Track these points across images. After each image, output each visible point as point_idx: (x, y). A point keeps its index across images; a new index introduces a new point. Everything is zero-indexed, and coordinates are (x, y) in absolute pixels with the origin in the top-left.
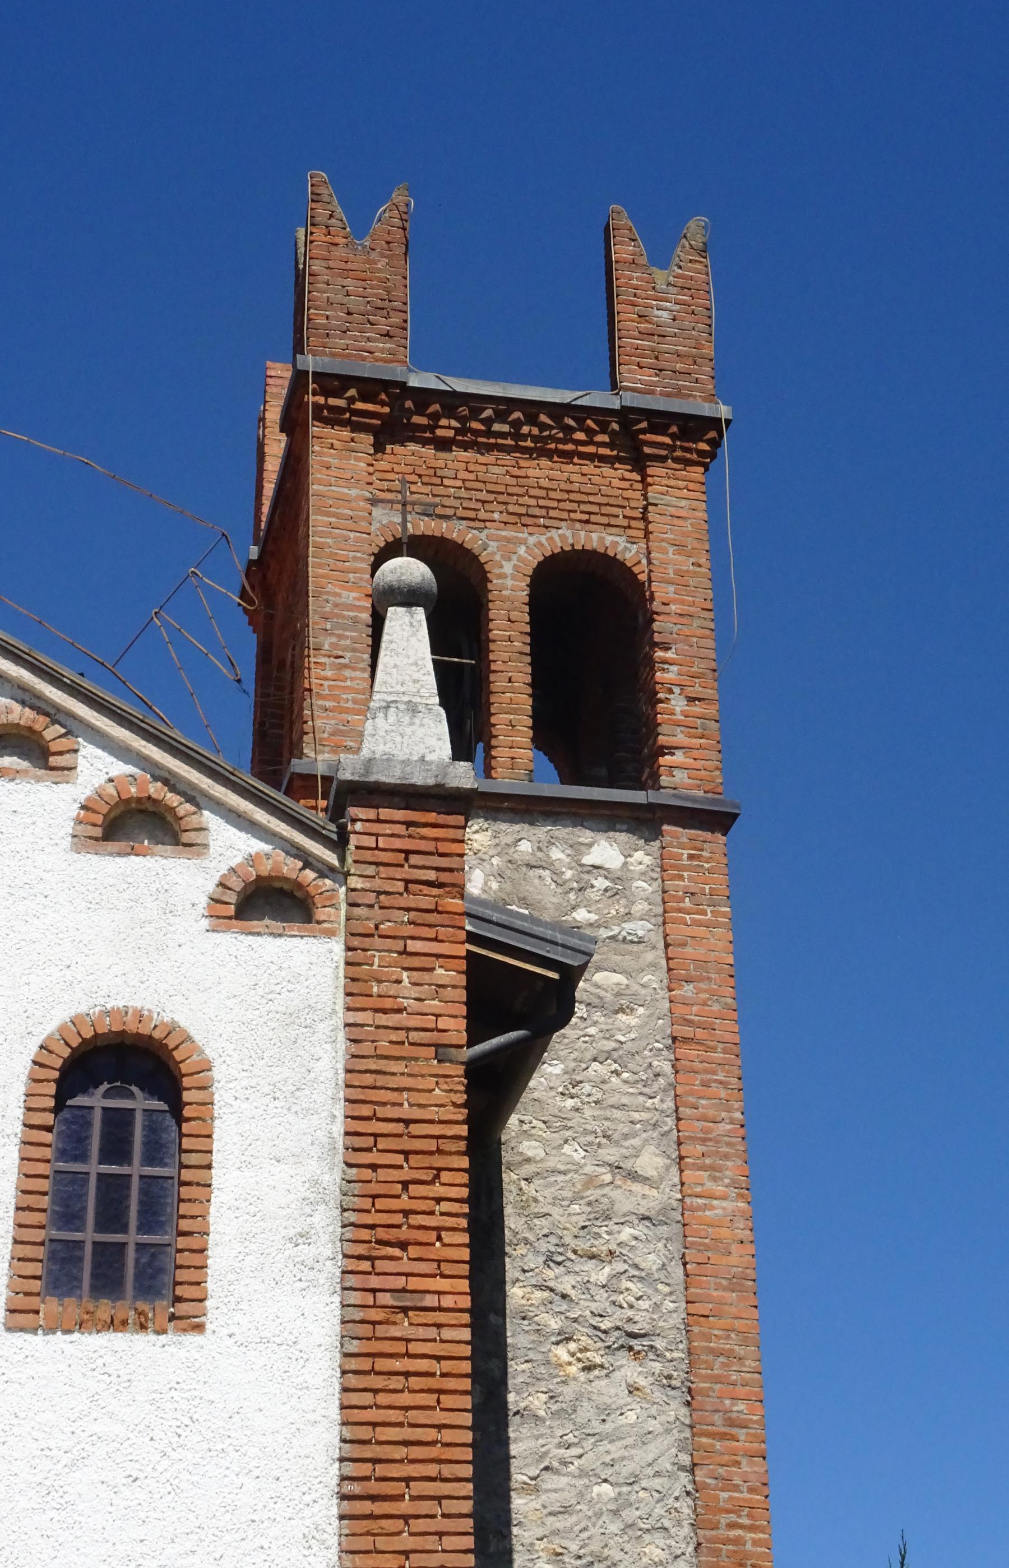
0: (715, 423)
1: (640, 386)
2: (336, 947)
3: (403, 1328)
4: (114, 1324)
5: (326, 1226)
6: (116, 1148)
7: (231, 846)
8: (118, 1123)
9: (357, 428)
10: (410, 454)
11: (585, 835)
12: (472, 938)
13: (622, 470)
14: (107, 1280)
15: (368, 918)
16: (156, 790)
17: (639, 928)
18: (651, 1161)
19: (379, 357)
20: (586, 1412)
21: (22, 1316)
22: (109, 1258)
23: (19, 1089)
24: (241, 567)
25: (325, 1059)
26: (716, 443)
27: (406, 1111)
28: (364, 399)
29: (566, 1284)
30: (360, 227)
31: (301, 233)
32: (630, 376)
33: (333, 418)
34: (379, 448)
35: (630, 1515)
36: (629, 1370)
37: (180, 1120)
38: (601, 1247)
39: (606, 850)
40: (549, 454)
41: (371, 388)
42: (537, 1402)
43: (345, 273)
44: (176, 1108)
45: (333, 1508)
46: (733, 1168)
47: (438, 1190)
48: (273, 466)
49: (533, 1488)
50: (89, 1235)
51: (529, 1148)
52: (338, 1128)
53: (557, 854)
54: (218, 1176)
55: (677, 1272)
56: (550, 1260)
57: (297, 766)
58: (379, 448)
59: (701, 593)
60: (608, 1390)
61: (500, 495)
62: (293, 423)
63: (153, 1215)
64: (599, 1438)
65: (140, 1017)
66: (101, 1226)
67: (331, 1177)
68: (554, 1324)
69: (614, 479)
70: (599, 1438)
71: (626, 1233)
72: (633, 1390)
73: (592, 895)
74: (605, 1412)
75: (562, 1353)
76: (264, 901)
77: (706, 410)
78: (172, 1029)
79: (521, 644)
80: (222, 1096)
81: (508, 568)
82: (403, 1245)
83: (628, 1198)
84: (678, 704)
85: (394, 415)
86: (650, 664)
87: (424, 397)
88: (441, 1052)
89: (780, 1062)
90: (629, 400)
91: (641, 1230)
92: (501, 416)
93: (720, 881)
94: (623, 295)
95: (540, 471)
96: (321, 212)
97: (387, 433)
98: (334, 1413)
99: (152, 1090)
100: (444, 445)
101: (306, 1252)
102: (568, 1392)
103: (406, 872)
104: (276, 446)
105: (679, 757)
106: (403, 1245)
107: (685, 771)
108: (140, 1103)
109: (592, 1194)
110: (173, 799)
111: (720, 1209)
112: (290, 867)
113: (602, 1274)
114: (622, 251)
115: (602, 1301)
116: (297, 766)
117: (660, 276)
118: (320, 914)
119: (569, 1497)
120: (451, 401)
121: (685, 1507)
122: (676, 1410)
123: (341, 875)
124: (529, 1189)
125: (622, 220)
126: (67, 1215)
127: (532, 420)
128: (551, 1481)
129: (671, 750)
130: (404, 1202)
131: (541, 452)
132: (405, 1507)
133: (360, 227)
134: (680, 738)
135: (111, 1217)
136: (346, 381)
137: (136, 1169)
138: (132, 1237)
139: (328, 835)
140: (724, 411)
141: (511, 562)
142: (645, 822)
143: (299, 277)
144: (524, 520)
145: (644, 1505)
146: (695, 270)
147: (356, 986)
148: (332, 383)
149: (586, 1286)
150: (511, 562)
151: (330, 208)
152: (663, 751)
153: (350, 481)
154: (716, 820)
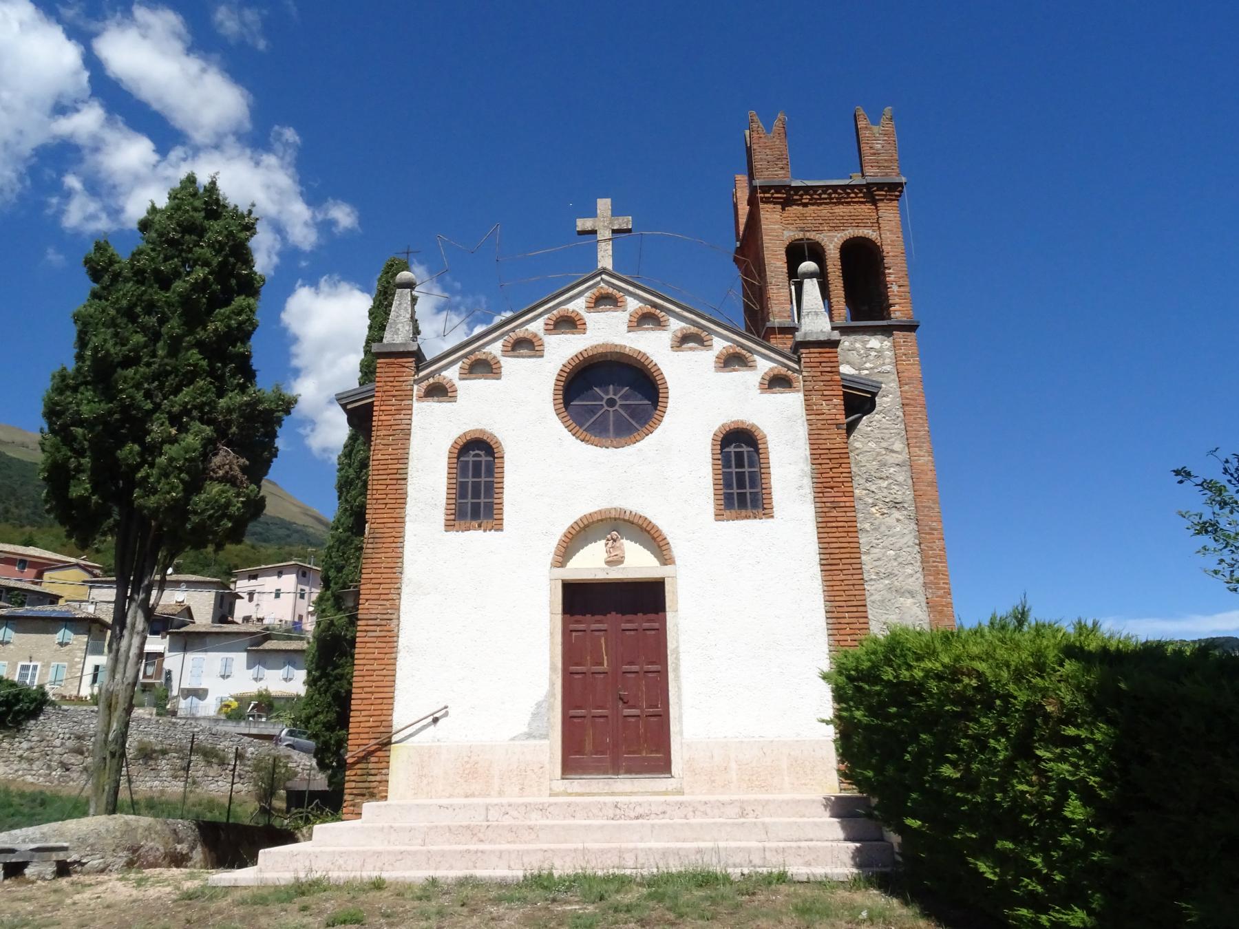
0: (901, 184)
1: (873, 174)
2: (801, 396)
3: (834, 513)
4: (747, 517)
5: (807, 483)
6: (740, 464)
7: (764, 365)
8: (739, 456)
9: (775, 203)
10: (795, 210)
11: (866, 338)
12: (844, 386)
13: (868, 206)
14: (742, 503)
15: (810, 385)
16: (738, 350)
17: (888, 368)
18: (898, 446)
19: (779, 176)
20: (883, 528)
21: (449, 526)
22: (742, 497)
23: (709, 448)
24: (733, 250)
25: (801, 431)
26: (901, 192)
27: (829, 446)
28: (777, 192)
29: (873, 488)
30: (769, 128)
31: (747, 132)
32: (869, 171)
33: (767, 201)
34: (783, 209)
35: (900, 560)
36: (896, 514)
37: (759, 454)
38: (884, 475)
39: (875, 342)
40: (842, 203)
41: (778, 189)
42: (867, 526)
43: (765, 147)
44: (757, 450)
45: (818, 568)
46: (926, 446)
47: (841, 470)
48: (743, 220)
49: (867, 553)
50: (735, 491)
51: (857, 445)
52: (808, 453)
53: (857, 345)
54: (772, 470)
55: (910, 481)
56: (867, 480)
57: (768, 324)
58: (783, 209)
59: (900, 247)
60: (890, 521)
61: (826, 220)
62: (752, 202)
63: (753, 484)
64: (888, 536)
65: (742, 422)
67: (807, 468)
68: (870, 501)
69: (866, 209)
70: (888, 536)
71: (892, 470)
72: (898, 520)
73: (871, 358)
74: (889, 528)
75: (873, 510)
76: (777, 382)
77: (897, 180)
78: (753, 425)
79: (839, 273)
80: (771, 446)
81: (831, 246)
82: (832, 488)
83: (892, 458)
84: (895, 288)
85: (788, 197)
86: (884, 275)
88: (838, 426)
89: (945, 416)
90: (870, 180)
91: (897, 469)
92: (824, 192)
93: (915, 349)
94: (863, 141)
95: (840, 210)
96: (755, 125)
97: (786, 203)
98: (816, 540)
99: (748, 445)
100: (805, 205)
101: (802, 492)
102: (877, 522)
103: (821, 369)
104: (744, 209)
105: (897, 307)
106: (832, 488)
107: (899, 313)
108: (745, 449)
109: (879, 458)
110: (744, 352)
111: (923, 460)
112: (783, 371)
113: (885, 484)
114: (861, 124)
115: (885, 492)
116: (768, 324)
117: (876, 129)
118: (795, 385)
119: (879, 555)
120: (807, 189)
121: (918, 556)
122: (913, 526)
123: (800, 372)
124: (858, 458)
125: (861, 112)
126: (728, 485)
127: (835, 192)
128: (874, 550)
129: (894, 305)
130: (831, 474)
131: (839, 203)
132: (841, 567)
133: (769, 128)
134: (897, 300)
135: (741, 484)
136: (771, 187)
137: (746, 469)
138: (748, 490)
139: (802, 360)
140: (904, 180)
141: (832, 244)
142: (887, 331)
143: (749, 151)
144: (835, 228)
145: (904, 556)
146: (889, 127)
148: (765, 189)
149: (880, 488)
150: (832, 244)
151: (758, 124)
152: (891, 305)
153: (775, 223)
154: (911, 328)
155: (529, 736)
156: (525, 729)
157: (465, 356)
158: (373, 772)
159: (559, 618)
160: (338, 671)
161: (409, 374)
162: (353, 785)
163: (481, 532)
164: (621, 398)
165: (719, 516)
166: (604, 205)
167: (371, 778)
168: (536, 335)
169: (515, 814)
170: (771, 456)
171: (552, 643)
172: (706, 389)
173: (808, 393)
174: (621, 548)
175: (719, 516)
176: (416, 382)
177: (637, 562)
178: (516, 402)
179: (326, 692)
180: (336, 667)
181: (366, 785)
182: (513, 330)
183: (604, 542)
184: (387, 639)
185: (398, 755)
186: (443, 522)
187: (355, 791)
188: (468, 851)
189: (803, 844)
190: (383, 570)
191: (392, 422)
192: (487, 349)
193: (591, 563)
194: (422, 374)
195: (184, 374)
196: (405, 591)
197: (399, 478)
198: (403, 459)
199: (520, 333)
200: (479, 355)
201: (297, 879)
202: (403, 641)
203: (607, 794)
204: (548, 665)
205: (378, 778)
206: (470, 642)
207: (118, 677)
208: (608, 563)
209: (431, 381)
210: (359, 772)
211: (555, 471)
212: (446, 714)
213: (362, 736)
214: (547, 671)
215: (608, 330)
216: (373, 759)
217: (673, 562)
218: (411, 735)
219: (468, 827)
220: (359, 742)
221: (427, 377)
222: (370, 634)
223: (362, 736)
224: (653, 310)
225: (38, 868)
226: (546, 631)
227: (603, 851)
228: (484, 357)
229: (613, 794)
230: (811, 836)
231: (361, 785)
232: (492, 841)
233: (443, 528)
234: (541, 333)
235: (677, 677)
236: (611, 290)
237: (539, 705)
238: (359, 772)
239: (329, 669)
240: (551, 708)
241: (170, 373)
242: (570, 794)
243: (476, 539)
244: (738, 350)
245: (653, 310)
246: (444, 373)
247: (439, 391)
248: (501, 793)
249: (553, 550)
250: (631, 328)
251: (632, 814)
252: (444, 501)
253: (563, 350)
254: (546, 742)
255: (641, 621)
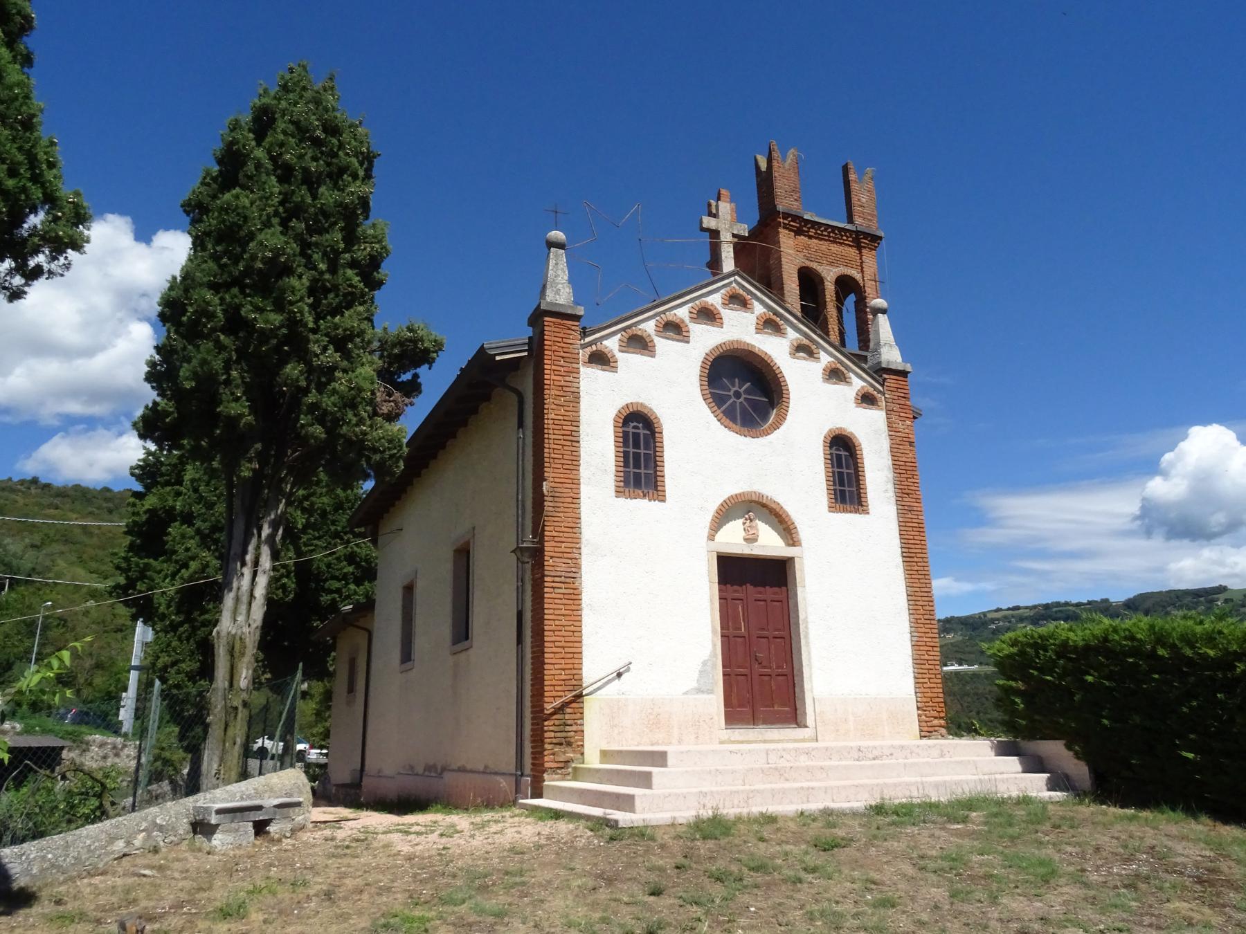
0: (881, 238)
5: (890, 487)
8: (636, 436)
15: (891, 406)
16: (839, 366)
21: (866, 512)
23: (821, 448)
32: (858, 220)
44: (653, 433)
52: (890, 462)
65: (646, 407)
66: (635, 467)
67: (891, 475)
69: (853, 252)
76: (867, 399)
80: (865, 452)
85: (802, 227)
87: (807, 221)
95: (835, 248)
97: (798, 232)
100: (810, 237)
112: (871, 390)
123: (884, 394)
140: (882, 234)
144: (831, 264)
146: (871, 185)
147: (890, 425)
155: (699, 691)
156: (695, 685)
157: (624, 329)
158: (569, 722)
159: (716, 586)
160: (207, 616)
161: (574, 339)
162: (552, 734)
163: (646, 501)
164: (745, 392)
165: (619, 493)
166: (725, 208)
167: (568, 728)
168: (683, 321)
169: (788, 757)
170: (612, 438)
171: (712, 609)
172: (819, 398)
173: (889, 413)
174: (756, 528)
175: (619, 493)
176: (584, 346)
177: (769, 543)
178: (665, 377)
179: (188, 639)
180: (205, 611)
181: (564, 734)
182: (664, 312)
183: (741, 521)
184: (573, 597)
185: (591, 707)
186: (613, 488)
187: (554, 741)
188: (802, 788)
189: (998, 776)
190: (563, 529)
191: (563, 383)
192: (642, 326)
193: (733, 538)
194: (588, 339)
195: (345, 295)
196: (584, 551)
197: (573, 440)
198: (575, 422)
199: (670, 316)
200: (634, 331)
201: (697, 817)
202: (586, 598)
203: (761, 742)
204: (710, 628)
205: (574, 728)
206: (637, 606)
207: (241, 618)
208: (745, 540)
209: (594, 348)
210: (557, 722)
211: (703, 452)
212: (628, 670)
213: (557, 688)
214: (710, 635)
215: (740, 328)
216: (568, 710)
217: (800, 545)
218: (599, 689)
219: (776, 769)
220: (554, 694)
221: (590, 344)
222: (557, 591)
223: (557, 688)
224: (774, 317)
225: (279, 826)
226: (707, 597)
227: (895, 785)
228: (639, 333)
229: (765, 742)
230: (1002, 770)
231: (559, 735)
232: (795, 780)
233: (613, 494)
234: (687, 320)
235: (807, 644)
236: (741, 292)
237: (704, 663)
238: (557, 722)
239: (196, 614)
240: (714, 666)
241: (329, 291)
242: (733, 742)
243: (641, 506)
244: (839, 366)
245: (774, 317)
246: (605, 342)
247: (601, 359)
248: (680, 742)
249: (708, 525)
250: (758, 331)
251: (871, 756)
252: (614, 468)
253: (705, 339)
254: (711, 696)
255: (770, 592)
